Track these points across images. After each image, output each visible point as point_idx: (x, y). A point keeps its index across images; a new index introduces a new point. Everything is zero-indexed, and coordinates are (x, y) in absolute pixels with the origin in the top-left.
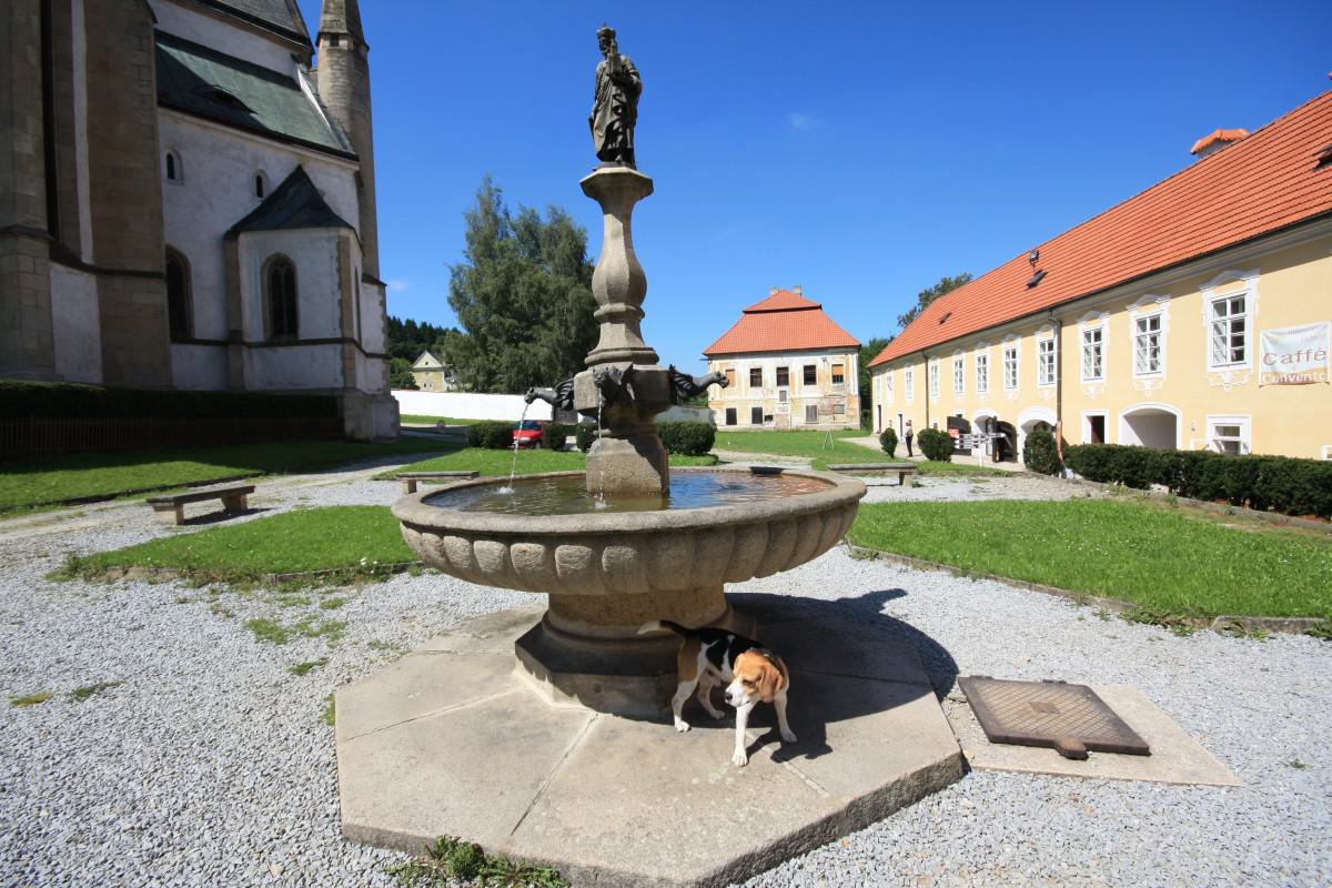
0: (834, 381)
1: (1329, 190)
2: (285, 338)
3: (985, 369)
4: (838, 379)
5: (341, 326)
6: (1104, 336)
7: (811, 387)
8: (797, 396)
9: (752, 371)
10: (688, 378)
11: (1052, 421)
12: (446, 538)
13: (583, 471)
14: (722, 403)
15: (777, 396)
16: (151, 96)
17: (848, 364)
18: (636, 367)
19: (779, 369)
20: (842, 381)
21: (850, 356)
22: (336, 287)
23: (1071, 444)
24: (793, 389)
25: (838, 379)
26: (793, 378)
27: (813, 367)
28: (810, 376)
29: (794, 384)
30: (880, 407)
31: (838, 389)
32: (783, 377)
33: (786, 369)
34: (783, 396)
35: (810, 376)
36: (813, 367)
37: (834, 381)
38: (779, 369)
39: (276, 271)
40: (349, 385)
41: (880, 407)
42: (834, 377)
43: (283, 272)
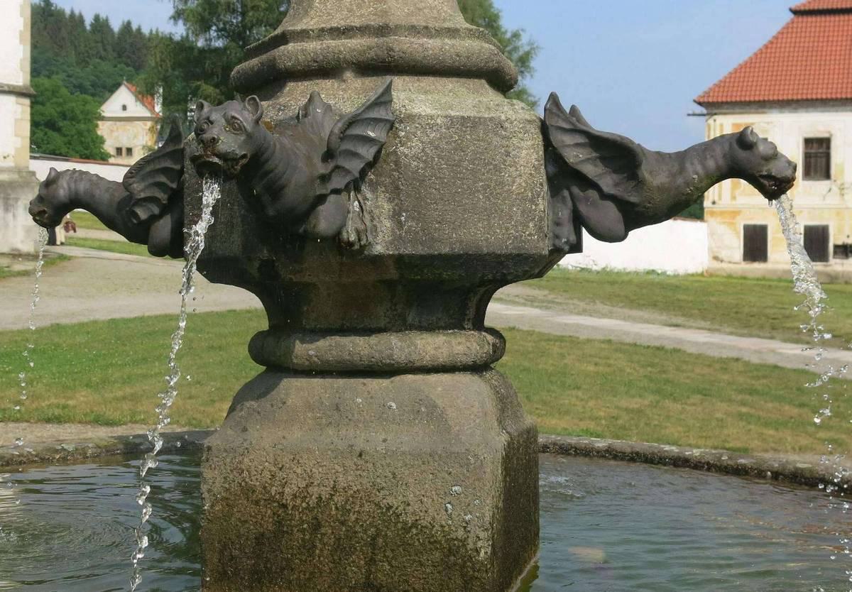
7: (822, 185)
9: (808, 142)
14: (735, 213)
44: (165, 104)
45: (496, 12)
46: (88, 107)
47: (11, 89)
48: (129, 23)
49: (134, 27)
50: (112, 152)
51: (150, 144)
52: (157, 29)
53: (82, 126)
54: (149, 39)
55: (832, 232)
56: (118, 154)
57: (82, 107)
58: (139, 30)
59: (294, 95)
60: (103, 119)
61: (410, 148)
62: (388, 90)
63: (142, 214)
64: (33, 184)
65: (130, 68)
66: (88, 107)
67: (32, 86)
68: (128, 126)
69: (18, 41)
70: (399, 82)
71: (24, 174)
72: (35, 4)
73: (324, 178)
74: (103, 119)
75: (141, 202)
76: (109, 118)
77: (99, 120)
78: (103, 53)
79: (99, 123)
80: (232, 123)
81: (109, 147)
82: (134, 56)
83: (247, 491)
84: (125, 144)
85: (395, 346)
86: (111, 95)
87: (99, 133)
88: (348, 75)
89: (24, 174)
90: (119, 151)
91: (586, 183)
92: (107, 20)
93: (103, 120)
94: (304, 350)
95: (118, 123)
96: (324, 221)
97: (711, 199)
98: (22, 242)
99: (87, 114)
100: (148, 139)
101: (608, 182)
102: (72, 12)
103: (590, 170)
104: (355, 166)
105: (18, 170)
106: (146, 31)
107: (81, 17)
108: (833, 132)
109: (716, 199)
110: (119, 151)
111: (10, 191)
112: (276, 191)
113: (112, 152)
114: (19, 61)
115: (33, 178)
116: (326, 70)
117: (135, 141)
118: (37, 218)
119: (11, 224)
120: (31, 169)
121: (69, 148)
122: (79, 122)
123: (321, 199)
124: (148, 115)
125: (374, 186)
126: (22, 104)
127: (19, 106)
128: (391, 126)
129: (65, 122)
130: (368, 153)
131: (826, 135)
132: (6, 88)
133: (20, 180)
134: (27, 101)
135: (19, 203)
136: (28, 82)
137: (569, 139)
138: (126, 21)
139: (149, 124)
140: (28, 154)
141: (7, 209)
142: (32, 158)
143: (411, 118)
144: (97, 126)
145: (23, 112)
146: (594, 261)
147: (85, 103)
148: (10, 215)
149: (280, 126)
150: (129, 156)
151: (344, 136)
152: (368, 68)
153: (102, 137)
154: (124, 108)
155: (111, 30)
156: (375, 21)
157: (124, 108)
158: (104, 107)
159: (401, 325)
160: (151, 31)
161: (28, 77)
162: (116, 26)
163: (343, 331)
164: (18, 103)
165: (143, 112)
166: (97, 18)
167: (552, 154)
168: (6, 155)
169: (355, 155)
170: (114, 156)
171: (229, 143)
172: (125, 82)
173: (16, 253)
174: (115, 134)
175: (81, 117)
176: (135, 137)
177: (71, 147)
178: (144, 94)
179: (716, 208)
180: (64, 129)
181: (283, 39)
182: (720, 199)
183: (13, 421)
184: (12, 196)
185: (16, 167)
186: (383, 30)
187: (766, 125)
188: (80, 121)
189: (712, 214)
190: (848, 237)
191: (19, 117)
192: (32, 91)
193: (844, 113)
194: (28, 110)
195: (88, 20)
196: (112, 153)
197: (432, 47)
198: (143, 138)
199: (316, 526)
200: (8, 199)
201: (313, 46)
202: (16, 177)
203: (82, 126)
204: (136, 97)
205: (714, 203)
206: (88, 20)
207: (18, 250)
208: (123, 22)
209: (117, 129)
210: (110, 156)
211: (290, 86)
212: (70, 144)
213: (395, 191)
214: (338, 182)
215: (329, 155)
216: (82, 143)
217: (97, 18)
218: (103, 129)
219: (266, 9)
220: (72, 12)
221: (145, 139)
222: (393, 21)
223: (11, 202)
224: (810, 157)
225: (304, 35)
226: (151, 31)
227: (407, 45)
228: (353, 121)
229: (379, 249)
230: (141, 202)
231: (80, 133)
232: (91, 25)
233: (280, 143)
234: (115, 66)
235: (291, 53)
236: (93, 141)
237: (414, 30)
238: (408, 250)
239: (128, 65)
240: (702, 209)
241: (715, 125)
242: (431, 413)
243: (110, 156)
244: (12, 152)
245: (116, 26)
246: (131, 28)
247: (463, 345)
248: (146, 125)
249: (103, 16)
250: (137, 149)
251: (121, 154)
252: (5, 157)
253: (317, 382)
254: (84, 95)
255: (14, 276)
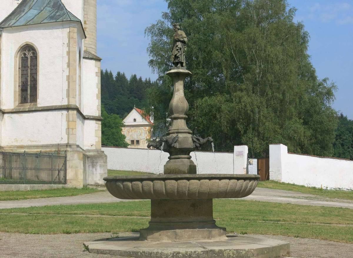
2: (27, 106)
5: (68, 96)
22: (65, 66)
39: (25, 54)
40: (71, 142)
43: (29, 55)
44: (155, 119)
46: (117, 121)
47: (94, 118)
48: (135, 76)
49: (138, 77)
50: (129, 142)
51: (148, 138)
52: (149, 78)
53: (114, 130)
54: (145, 84)
56: (132, 144)
57: (113, 121)
58: (140, 79)
59: (171, 135)
60: (125, 126)
61: (180, 139)
62: (178, 135)
63: (158, 146)
64: (103, 156)
65: (137, 99)
66: (117, 121)
67: (102, 116)
68: (137, 129)
69: (96, 98)
70: (179, 134)
71: (100, 152)
73: (173, 142)
74: (125, 126)
75: (158, 145)
76: (127, 125)
77: (123, 127)
78: (122, 92)
79: (123, 128)
80: (165, 138)
81: (128, 140)
82: (138, 93)
83: (168, 169)
84: (135, 138)
85: (180, 156)
86: (129, 113)
87: (123, 133)
88: (175, 133)
89: (100, 152)
90: (133, 142)
91: (196, 142)
92: (124, 75)
93: (124, 127)
94: (172, 157)
95: (132, 128)
96: (173, 145)
98: (99, 180)
99: (117, 124)
100: (147, 136)
101: (198, 142)
102: (106, 71)
103: (196, 141)
104: (175, 141)
105: (97, 151)
106: (143, 80)
107: (111, 73)
110: (133, 142)
111: (94, 159)
112: (168, 143)
113: (129, 142)
114: (96, 106)
115: (103, 154)
116: (173, 133)
117: (140, 137)
119: (95, 172)
120: (102, 150)
121: (108, 142)
122: (112, 128)
123: (172, 144)
124: (147, 123)
125: (177, 143)
126: (98, 124)
127: (97, 124)
128: (178, 138)
129: (105, 128)
130: (176, 140)
132: (92, 117)
133: (98, 155)
134: (100, 123)
135: (98, 164)
136: (100, 114)
137: (194, 138)
138: (133, 74)
139: (147, 128)
140: (101, 145)
141: (93, 167)
142: (102, 147)
143: (180, 137)
144: (121, 130)
145: (99, 127)
147: (116, 118)
148: (94, 169)
149: (169, 138)
150: (138, 145)
151: (174, 138)
152: (177, 133)
153: (124, 135)
154: (135, 120)
155: (126, 80)
156: (177, 129)
157: (135, 120)
158: (124, 120)
159: (181, 154)
160: (146, 79)
161: (100, 112)
162: (128, 77)
163: (176, 155)
164: (96, 123)
165: (146, 123)
166: (119, 74)
167: (193, 140)
168: (92, 145)
169: (175, 140)
170: (130, 145)
171: (165, 140)
172: (135, 107)
173: (97, 184)
174: (131, 133)
175: (113, 125)
176: (140, 135)
177: (109, 141)
178: (145, 116)
180: (105, 132)
181: (170, 130)
184: (95, 161)
185: (96, 149)
186: (178, 130)
188: (113, 127)
191: (97, 129)
192: (102, 118)
194: (100, 126)
195: (115, 75)
196: (129, 143)
197: (182, 131)
198: (145, 135)
199: (173, 171)
200: (93, 162)
201: (172, 131)
202: (96, 153)
203: (114, 130)
204: (142, 116)
206: (115, 75)
207: (98, 184)
208: (132, 76)
209: (132, 131)
210: (129, 145)
211: (171, 134)
212: (109, 139)
213: (178, 143)
214: (173, 142)
215: (173, 140)
216: (114, 138)
217: (119, 74)
218: (125, 131)
219: (202, 75)
220: (106, 71)
221: (145, 136)
222: (179, 129)
223: (94, 164)
225: (172, 130)
226: (146, 79)
227: (180, 131)
228: (175, 138)
229: (177, 148)
230: (158, 145)
231: (113, 134)
232: (116, 78)
233: (169, 139)
234: (129, 98)
235: (170, 132)
236: (120, 138)
237: (181, 129)
238: (180, 148)
239: (135, 97)
242: (182, 161)
243: (129, 145)
244: (95, 144)
245: (128, 77)
246: (136, 78)
247: (186, 156)
248: (146, 128)
249: (122, 73)
250: (142, 140)
251: (134, 144)
252: (92, 146)
253: (173, 160)
254: (115, 115)
255: (99, 191)
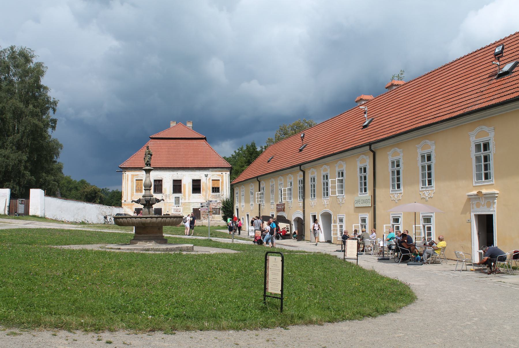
0: (213, 191)
1: (517, 77)
3: (314, 185)
4: (216, 190)
6: (433, 157)
7: (196, 195)
8: (187, 201)
10: (158, 199)
11: (302, 217)
12: (147, 219)
13: (213, 194)
15: (173, 200)
16: (133, 175)
17: (223, 179)
18: (398, 245)
19: (174, 181)
20: (218, 191)
21: (224, 173)
23: (65, 176)
24: (185, 196)
25: (216, 190)
26: (185, 188)
27: (199, 181)
28: (196, 187)
29: (185, 192)
30: (238, 209)
31: (216, 197)
32: (177, 186)
33: (180, 181)
34: (177, 199)
35: (196, 187)
36: (199, 181)
37: (213, 191)
38: (174, 181)
41: (238, 209)
42: (213, 188)
45: (480, 207)
55: (163, 210)
72: (58, 154)
97: (124, 200)
108: (163, 178)
109: (126, 200)
118: (25, 229)
131: (161, 179)
144: (278, 223)
146: (87, 221)
179: (126, 203)
182: (127, 200)
183: (469, 325)
187: (142, 175)
189: (125, 205)
190: (168, 212)
193: (167, 172)
205: (125, 201)
224: (156, 186)
240: (121, 203)
241: (126, 175)
